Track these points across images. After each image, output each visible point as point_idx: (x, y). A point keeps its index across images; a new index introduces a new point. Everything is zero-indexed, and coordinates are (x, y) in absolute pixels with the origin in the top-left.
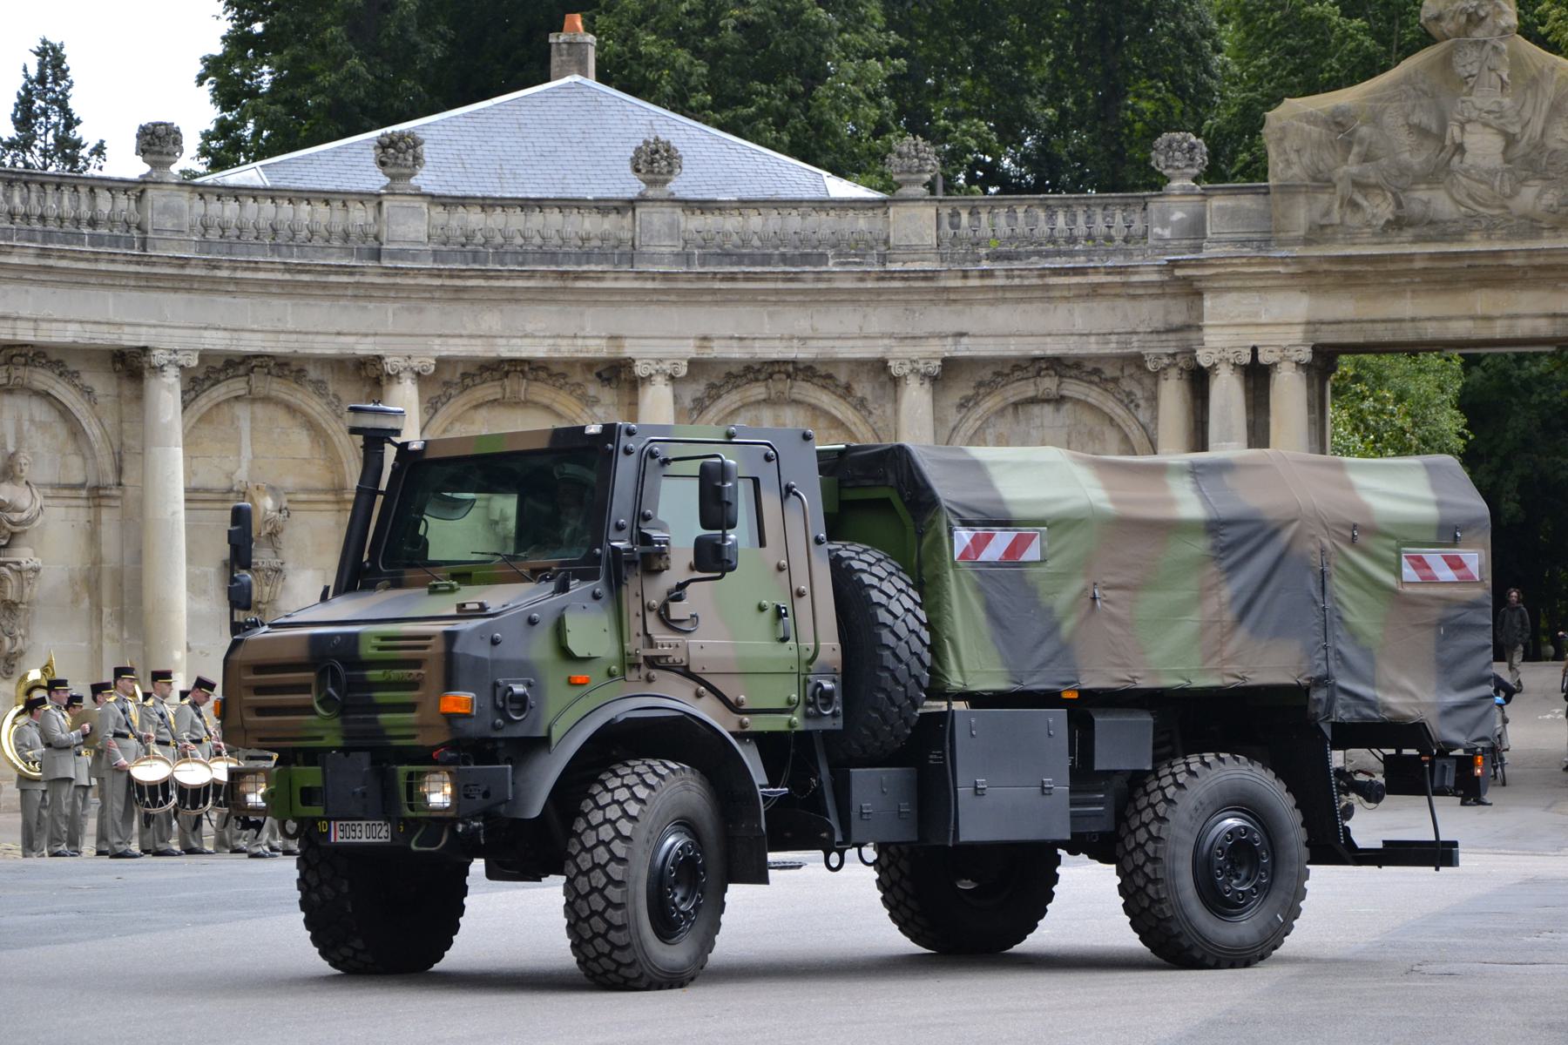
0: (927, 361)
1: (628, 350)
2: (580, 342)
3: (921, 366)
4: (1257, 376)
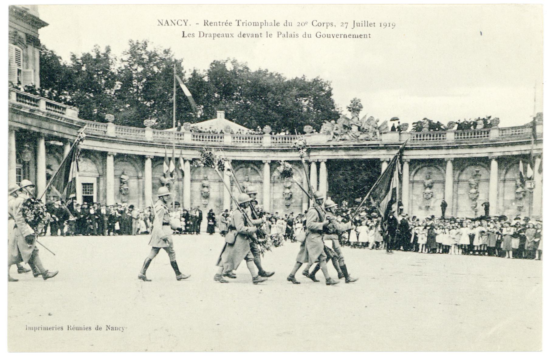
4: (318, 164)
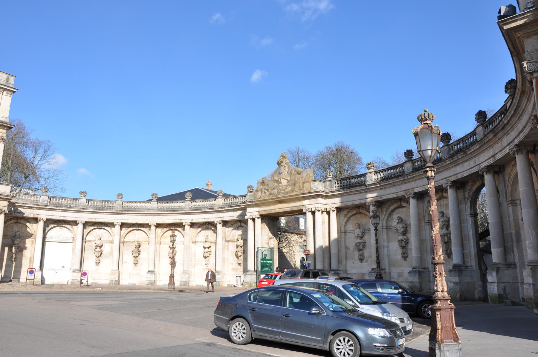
0: (188, 223)
1: (183, 221)
2: (176, 220)
3: (219, 222)
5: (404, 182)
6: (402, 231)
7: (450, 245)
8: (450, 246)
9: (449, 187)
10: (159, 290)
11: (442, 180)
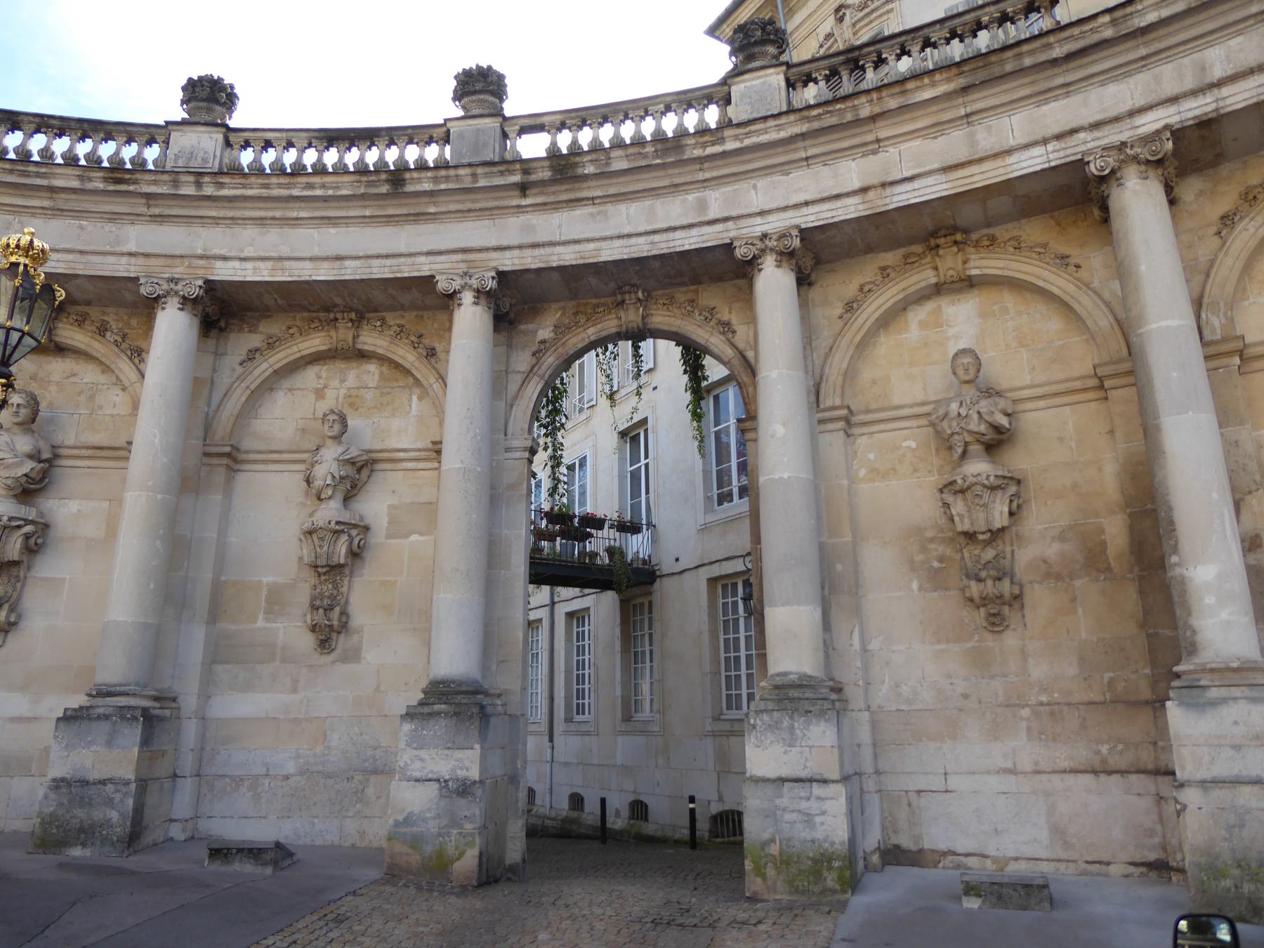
5: (156, 211)
6: (26, 475)
7: (346, 582)
8: (345, 589)
9: (468, 297)
10: (88, 448)
11: (429, 253)
